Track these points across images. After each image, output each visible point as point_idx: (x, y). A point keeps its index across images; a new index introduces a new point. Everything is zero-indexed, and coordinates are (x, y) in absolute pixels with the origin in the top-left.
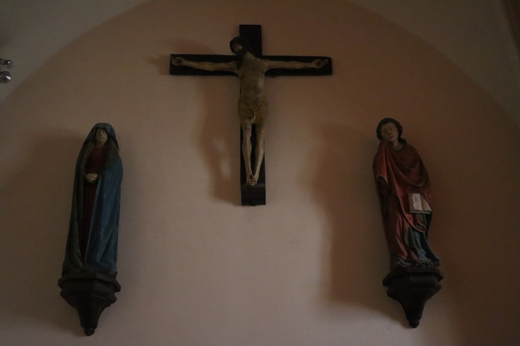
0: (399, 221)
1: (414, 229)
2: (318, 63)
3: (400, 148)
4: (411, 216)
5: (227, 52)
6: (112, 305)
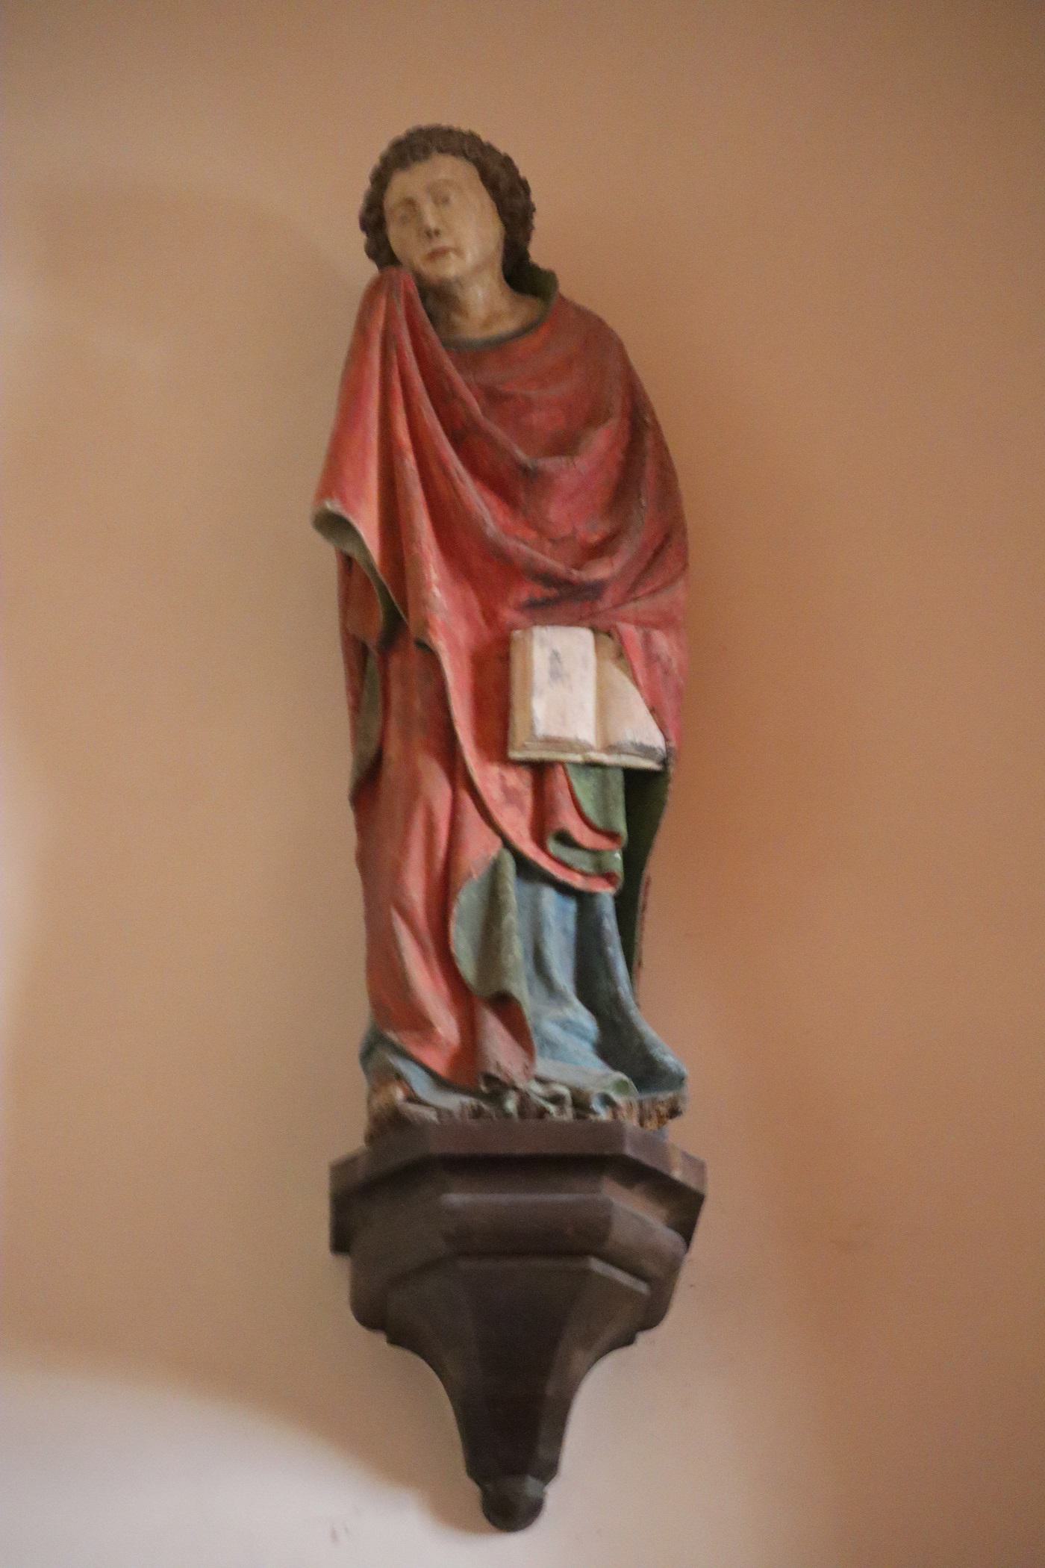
0: (430, 814)
1: (526, 869)
3: (508, 325)
4: (520, 781)
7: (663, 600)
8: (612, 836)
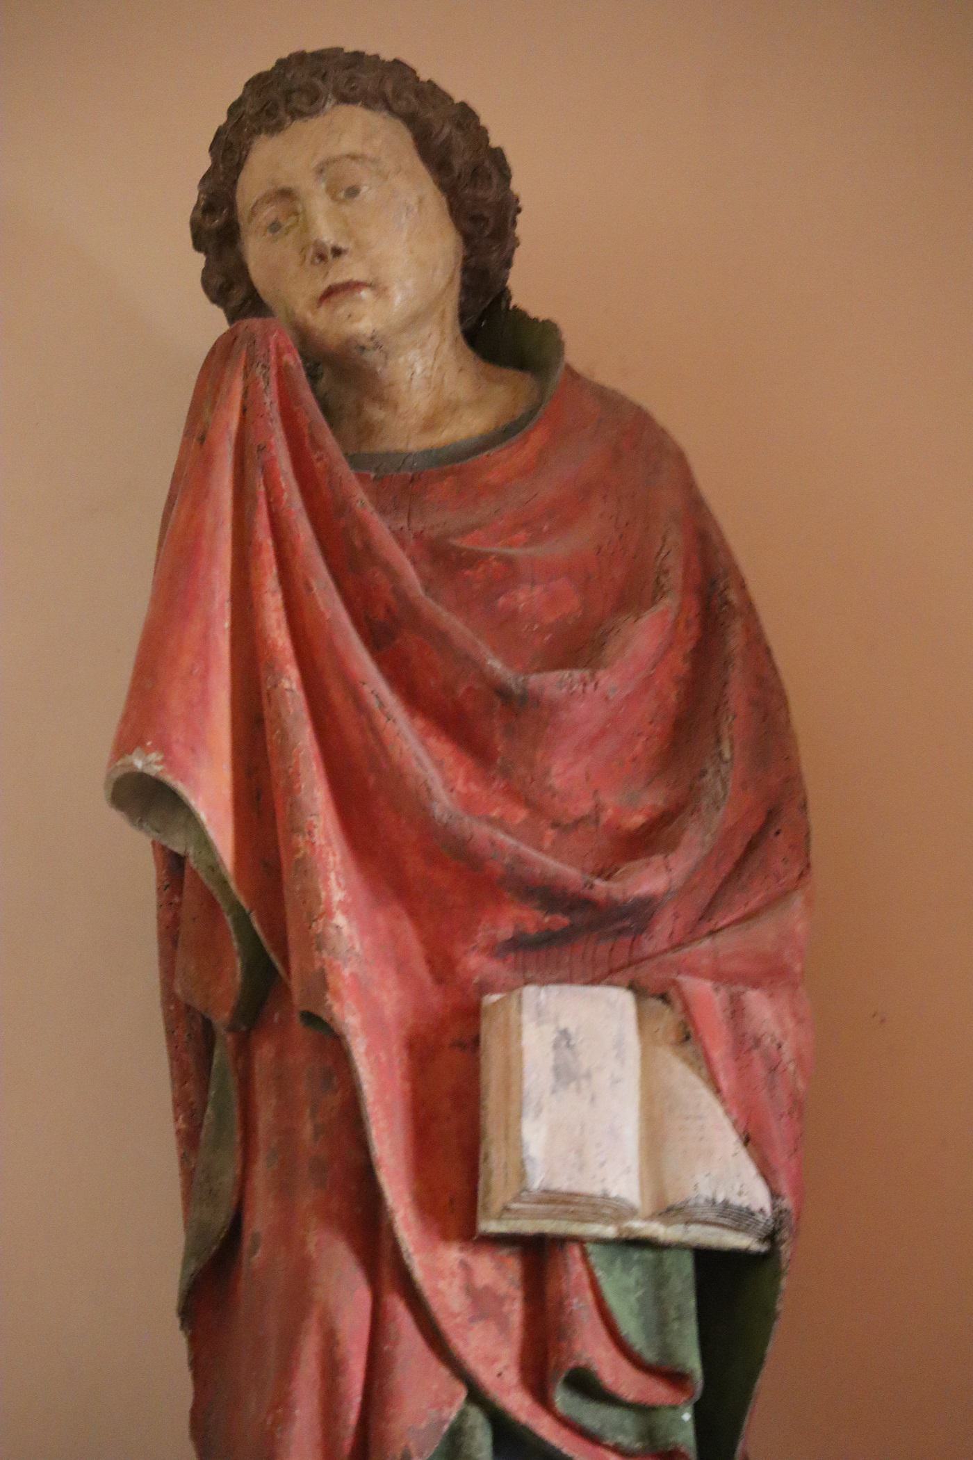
0: (330, 1339)
3: (471, 425)
4: (499, 1275)
7: (765, 933)
8: (675, 1378)
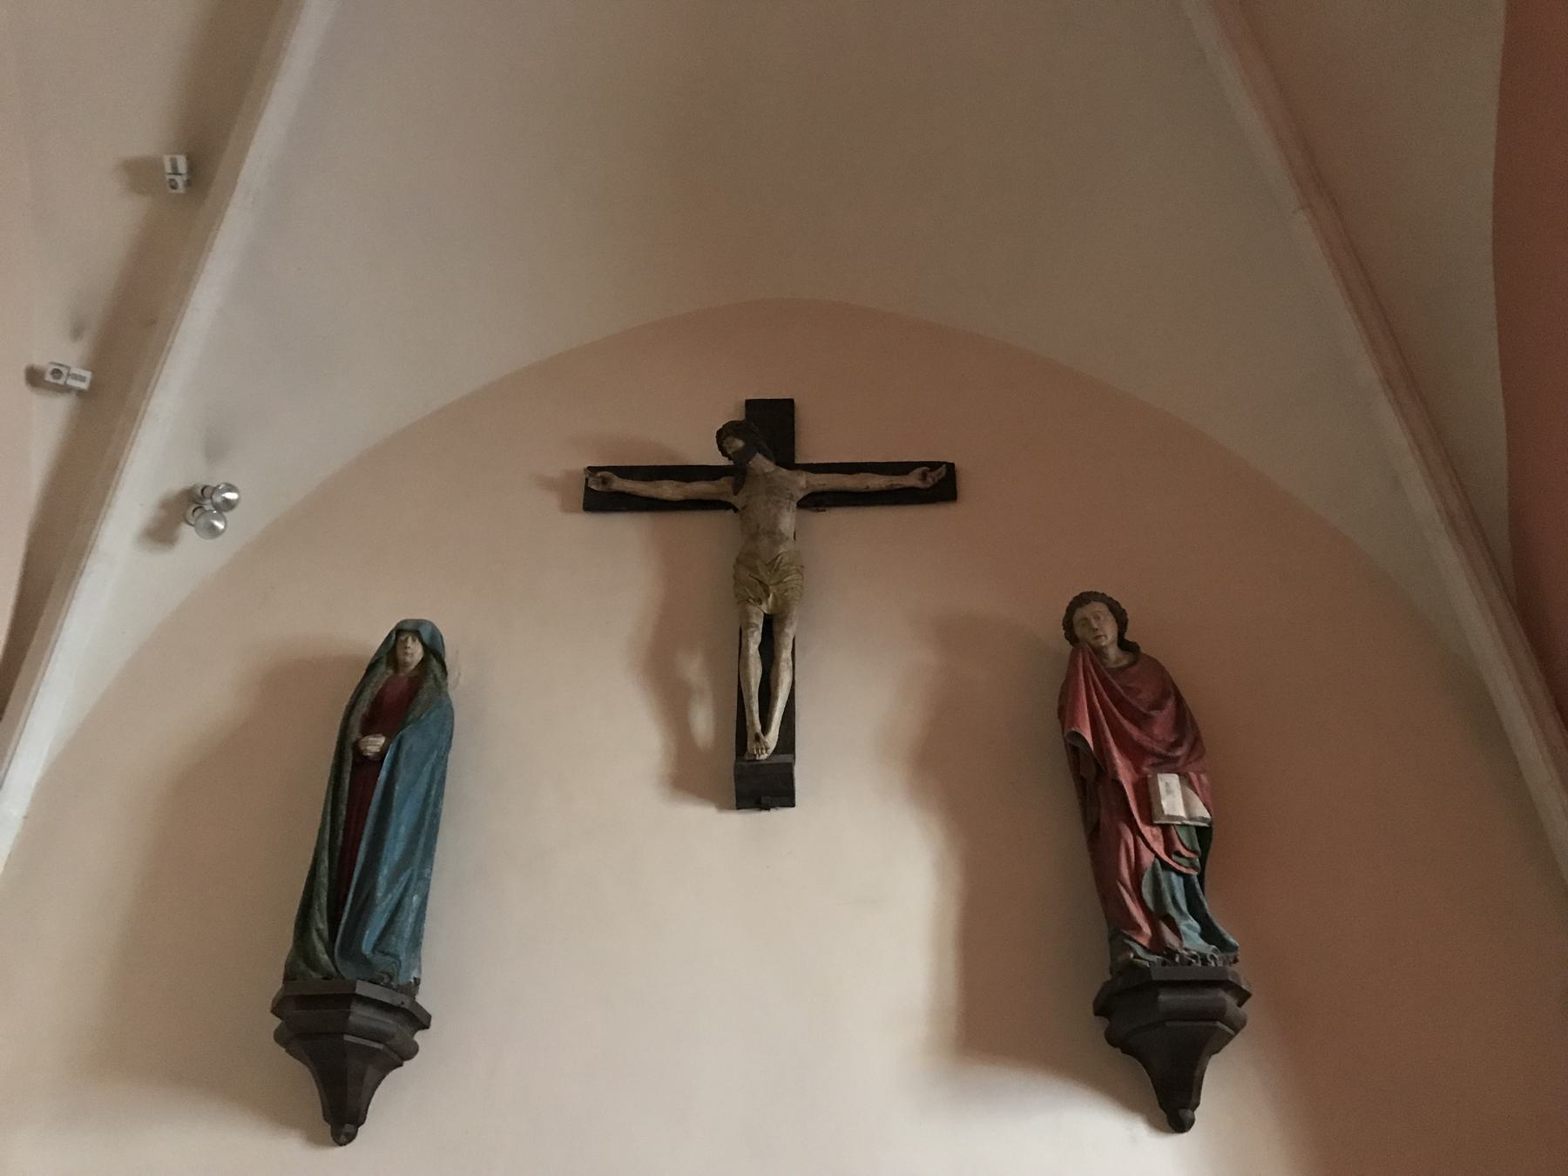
1: (1165, 866)
2: (924, 477)
3: (1125, 662)
4: (1157, 831)
5: (713, 457)
6: (406, 1063)
